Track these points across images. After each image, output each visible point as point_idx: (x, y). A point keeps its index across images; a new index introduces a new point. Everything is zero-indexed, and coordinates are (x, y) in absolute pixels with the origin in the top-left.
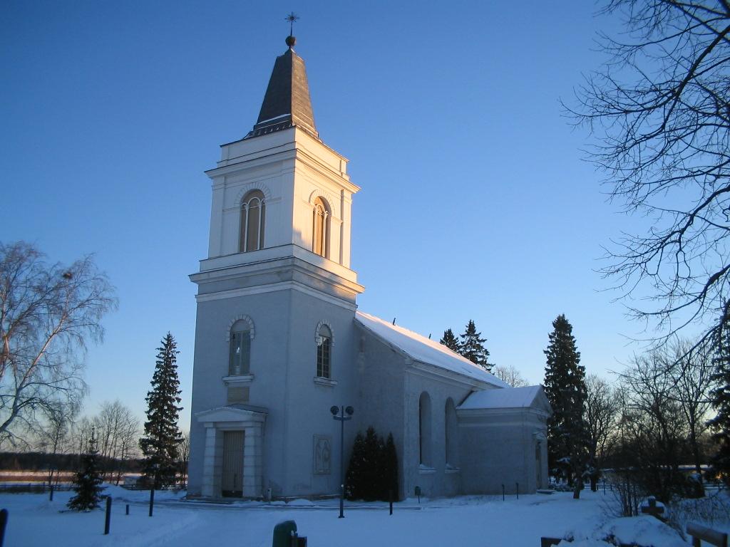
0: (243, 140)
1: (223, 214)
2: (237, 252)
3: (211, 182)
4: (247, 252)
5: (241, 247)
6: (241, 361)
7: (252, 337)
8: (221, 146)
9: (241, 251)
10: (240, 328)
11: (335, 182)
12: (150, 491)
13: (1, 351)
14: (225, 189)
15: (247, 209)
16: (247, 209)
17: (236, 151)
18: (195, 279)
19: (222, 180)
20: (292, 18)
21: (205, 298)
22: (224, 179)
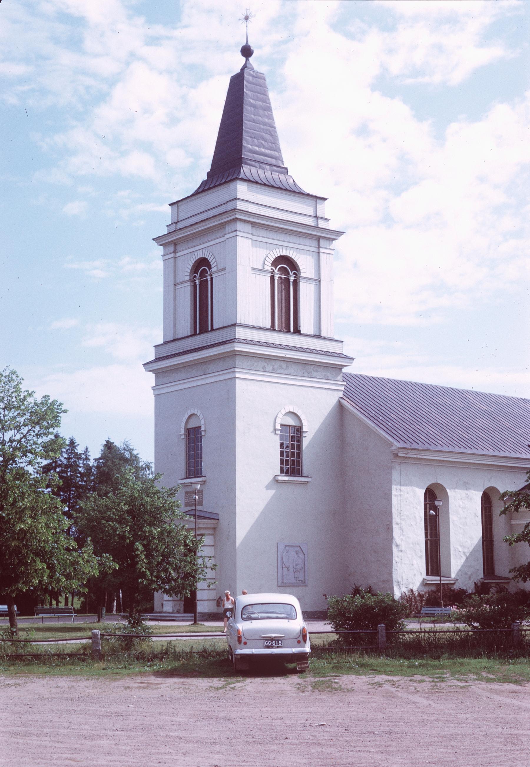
0: (193, 195)
1: (175, 290)
2: (189, 334)
4: (201, 333)
5: (297, 293)
6: (106, 605)
7: (203, 433)
8: (253, 269)
9: (195, 334)
10: (192, 425)
11: (295, 385)
12: (270, 327)
13: (2, 439)
14: (175, 258)
15: (197, 282)
16: (197, 282)
17: (186, 211)
18: (151, 369)
19: (172, 249)
20: (247, 18)
21: (157, 392)
22: (173, 246)
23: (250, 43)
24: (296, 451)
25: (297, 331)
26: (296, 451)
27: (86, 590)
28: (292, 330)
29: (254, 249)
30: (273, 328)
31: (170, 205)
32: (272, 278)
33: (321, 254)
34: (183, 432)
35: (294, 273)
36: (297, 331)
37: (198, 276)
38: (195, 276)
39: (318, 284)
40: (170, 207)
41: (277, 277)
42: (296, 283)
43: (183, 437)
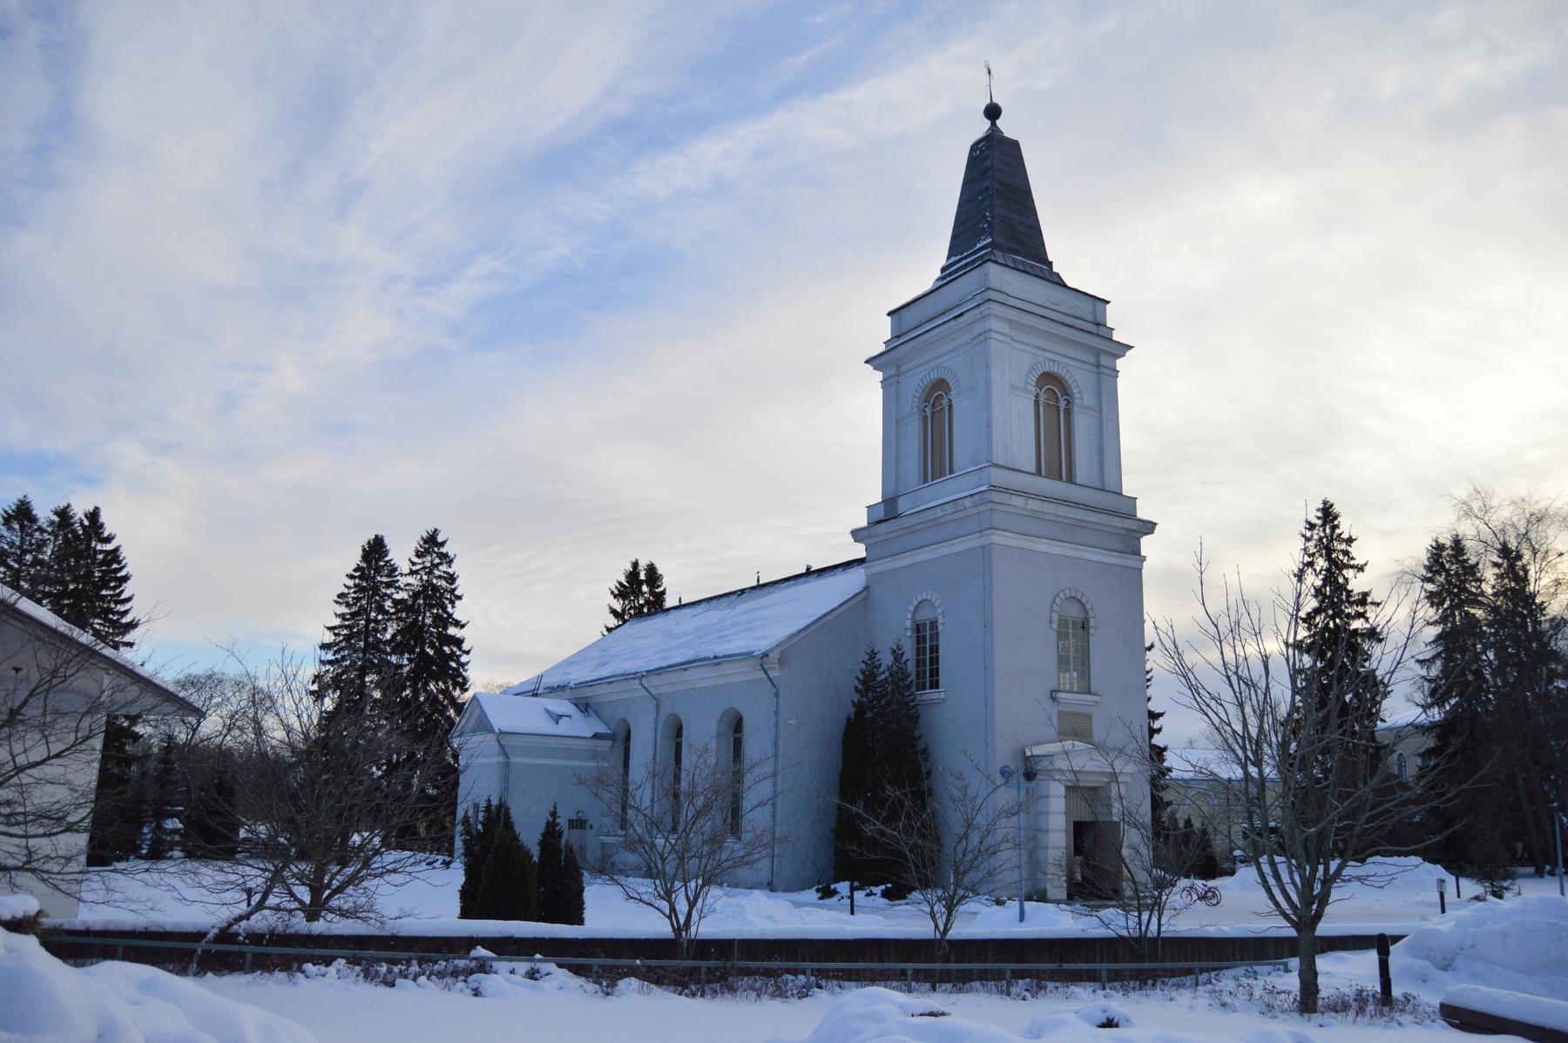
3: (879, 375)
10: (925, 615)
17: (911, 318)
23: (994, 101)
24: (1063, 630)
25: (1071, 479)
26: (1063, 630)
27: (1264, 859)
28: (1064, 478)
29: (797, 910)
30: (1039, 473)
31: (889, 314)
32: (1037, 402)
33: (1103, 376)
34: (909, 624)
35: (1066, 399)
36: (1071, 479)
37: (929, 405)
38: (926, 406)
39: (1098, 415)
40: (889, 318)
41: (1042, 399)
42: (1068, 412)
43: (909, 633)
